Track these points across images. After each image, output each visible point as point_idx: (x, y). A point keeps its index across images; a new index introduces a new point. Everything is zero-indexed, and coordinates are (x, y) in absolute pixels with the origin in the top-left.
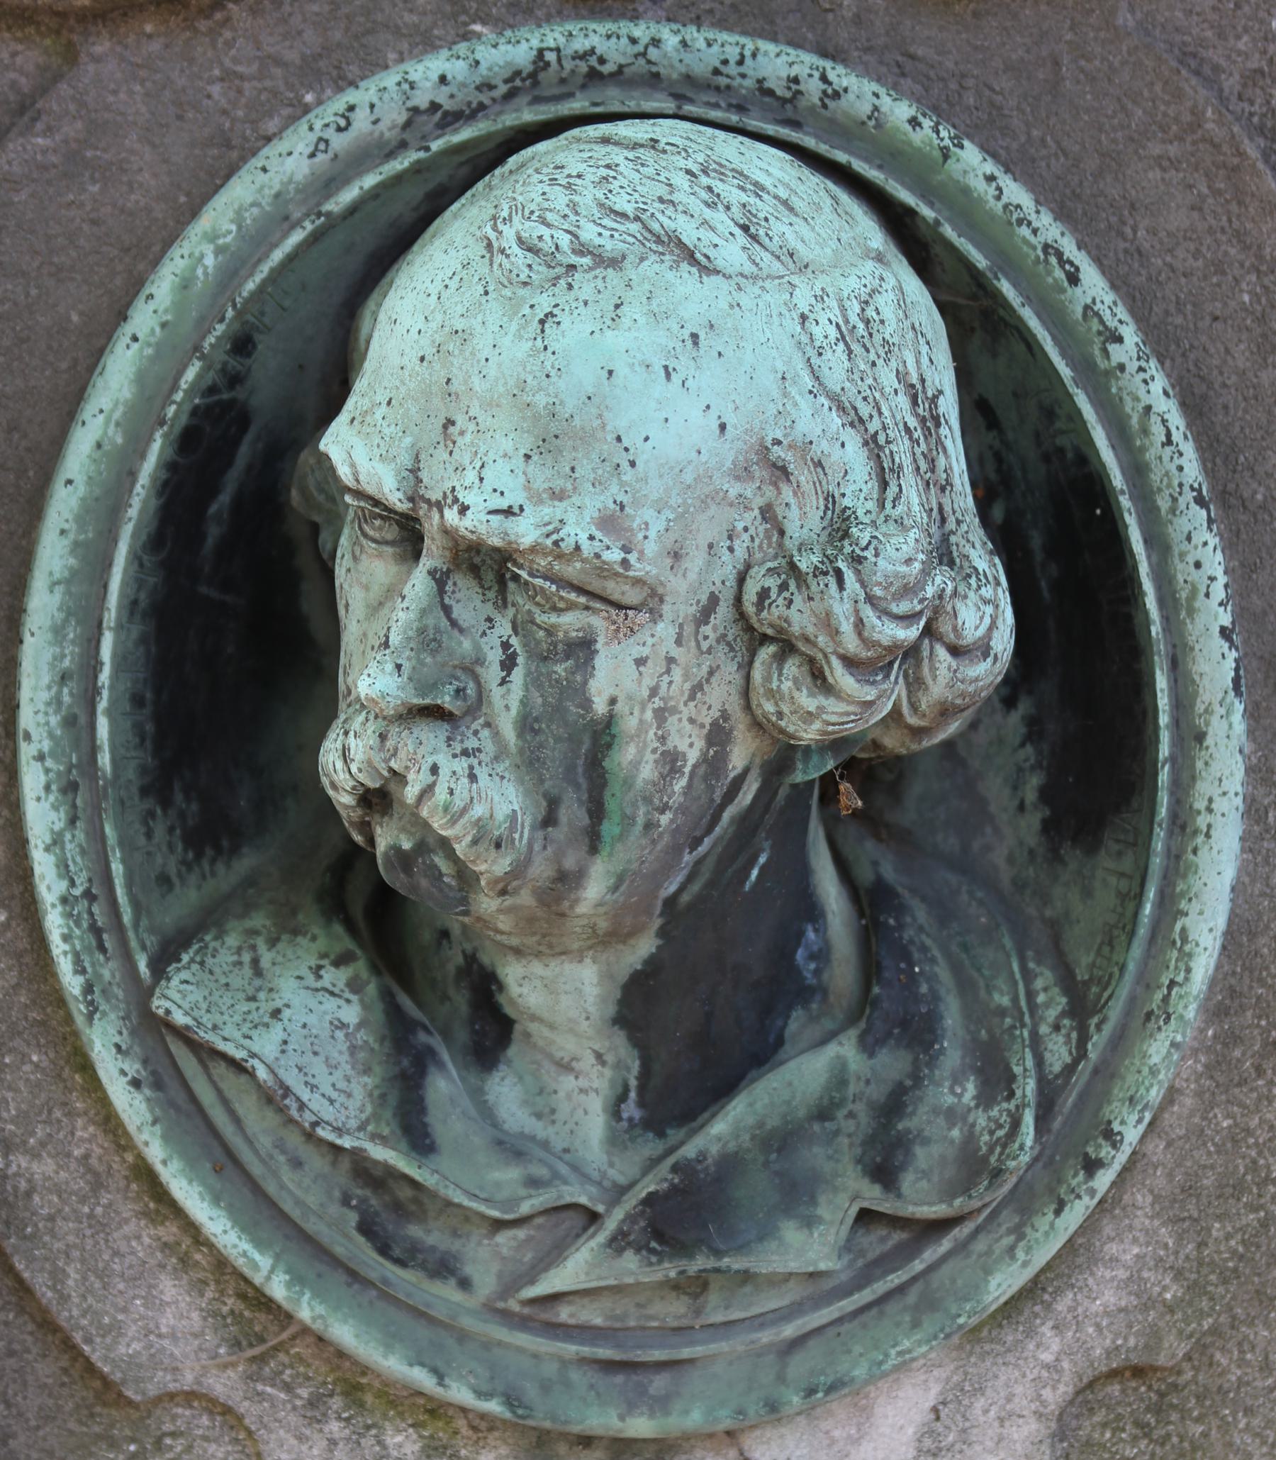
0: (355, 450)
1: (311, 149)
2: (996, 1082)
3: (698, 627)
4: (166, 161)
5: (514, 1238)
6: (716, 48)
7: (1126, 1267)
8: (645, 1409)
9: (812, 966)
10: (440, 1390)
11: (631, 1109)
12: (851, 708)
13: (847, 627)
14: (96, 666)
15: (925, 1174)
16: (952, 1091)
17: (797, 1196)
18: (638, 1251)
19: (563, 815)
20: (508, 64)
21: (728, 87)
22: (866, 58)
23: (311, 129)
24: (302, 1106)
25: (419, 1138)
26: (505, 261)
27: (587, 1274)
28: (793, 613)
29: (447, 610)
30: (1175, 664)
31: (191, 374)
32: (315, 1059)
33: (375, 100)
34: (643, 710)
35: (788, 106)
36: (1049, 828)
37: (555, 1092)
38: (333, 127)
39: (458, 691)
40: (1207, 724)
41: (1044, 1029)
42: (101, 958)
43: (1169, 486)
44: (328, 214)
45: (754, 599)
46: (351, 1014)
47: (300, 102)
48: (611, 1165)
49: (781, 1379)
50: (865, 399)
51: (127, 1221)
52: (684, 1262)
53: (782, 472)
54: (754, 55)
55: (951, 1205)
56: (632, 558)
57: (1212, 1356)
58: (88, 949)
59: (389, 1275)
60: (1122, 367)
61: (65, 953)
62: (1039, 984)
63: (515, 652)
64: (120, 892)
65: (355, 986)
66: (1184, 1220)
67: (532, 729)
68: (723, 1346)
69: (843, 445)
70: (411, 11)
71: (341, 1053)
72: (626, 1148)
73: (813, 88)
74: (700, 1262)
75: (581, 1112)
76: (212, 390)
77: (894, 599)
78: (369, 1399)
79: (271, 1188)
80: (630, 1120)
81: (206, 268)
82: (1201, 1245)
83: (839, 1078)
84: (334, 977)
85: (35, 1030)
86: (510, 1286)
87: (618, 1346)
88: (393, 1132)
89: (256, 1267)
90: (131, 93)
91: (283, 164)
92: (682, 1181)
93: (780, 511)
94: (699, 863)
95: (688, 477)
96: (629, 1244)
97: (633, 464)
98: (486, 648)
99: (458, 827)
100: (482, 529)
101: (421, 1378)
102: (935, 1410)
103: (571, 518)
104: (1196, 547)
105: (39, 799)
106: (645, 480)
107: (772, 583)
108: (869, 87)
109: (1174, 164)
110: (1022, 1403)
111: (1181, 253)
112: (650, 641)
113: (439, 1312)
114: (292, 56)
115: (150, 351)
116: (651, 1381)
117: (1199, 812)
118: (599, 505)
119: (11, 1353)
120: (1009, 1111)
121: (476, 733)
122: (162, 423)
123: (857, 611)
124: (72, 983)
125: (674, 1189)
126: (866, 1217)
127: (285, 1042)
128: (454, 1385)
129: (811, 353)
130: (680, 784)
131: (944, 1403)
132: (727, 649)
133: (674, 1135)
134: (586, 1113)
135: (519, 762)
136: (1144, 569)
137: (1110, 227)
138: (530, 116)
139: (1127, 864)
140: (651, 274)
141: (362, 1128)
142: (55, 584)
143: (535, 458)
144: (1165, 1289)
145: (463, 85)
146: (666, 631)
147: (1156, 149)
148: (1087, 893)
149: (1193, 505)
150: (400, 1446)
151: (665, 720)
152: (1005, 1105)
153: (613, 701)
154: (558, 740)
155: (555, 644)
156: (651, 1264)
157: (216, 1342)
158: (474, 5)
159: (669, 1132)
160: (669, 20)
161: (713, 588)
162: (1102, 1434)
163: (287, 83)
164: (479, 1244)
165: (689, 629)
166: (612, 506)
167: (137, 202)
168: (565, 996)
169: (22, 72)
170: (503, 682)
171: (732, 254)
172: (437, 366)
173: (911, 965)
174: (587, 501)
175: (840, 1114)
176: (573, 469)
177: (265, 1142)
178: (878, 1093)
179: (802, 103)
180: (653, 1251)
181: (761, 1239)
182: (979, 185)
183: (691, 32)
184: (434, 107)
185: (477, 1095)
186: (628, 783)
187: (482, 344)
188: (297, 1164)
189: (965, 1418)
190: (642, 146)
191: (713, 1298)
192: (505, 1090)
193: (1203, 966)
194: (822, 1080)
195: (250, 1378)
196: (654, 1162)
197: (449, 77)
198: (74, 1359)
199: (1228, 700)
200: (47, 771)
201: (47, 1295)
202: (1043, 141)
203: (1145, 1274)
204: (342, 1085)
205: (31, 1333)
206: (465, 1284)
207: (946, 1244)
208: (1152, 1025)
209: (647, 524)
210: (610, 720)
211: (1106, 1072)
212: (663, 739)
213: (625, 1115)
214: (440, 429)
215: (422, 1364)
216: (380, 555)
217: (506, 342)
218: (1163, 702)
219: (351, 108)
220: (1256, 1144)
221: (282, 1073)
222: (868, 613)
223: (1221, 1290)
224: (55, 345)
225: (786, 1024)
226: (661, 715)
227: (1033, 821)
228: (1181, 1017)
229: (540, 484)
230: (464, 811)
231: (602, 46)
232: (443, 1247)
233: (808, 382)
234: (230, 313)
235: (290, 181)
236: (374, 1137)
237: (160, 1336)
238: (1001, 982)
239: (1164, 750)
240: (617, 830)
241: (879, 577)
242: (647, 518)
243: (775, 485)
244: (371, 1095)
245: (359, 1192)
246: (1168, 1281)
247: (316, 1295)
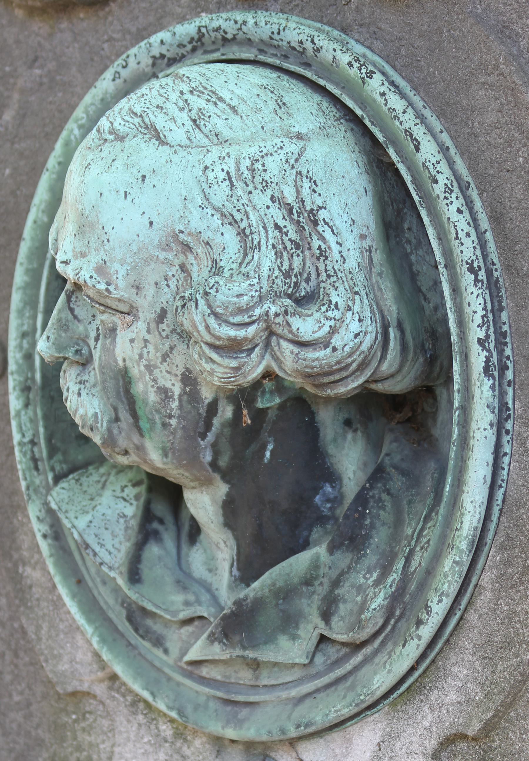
1: (112, 77)
3: (158, 325)
5: (188, 631)
6: (269, 26)
8: (233, 725)
9: (328, 505)
12: (227, 370)
13: (202, 328)
15: (342, 618)
17: (289, 623)
18: (219, 643)
20: (187, 34)
22: (360, 30)
24: (95, 554)
27: (201, 652)
29: (72, 310)
32: (106, 532)
34: (139, 365)
39: (77, 351)
42: (35, 473)
49: (289, 717)
50: (238, 211)
53: (187, 248)
54: (284, 29)
56: (111, 288)
57: (508, 734)
58: (29, 469)
66: (486, 658)
69: (222, 234)
70: (179, 6)
71: (120, 529)
72: (234, 591)
77: (232, 315)
81: (75, 136)
82: (494, 672)
83: (315, 565)
84: (131, 492)
87: (228, 692)
92: (236, 609)
93: (189, 267)
94: (214, 446)
95: (134, 248)
97: (108, 241)
98: (90, 330)
101: (146, 695)
102: (379, 745)
106: (113, 249)
110: (415, 747)
111: (494, 135)
112: (136, 331)
114: (134, 29)
115: (54, 176)
116: (241, 711)
118: (96, 261)
123: (205, 320)
127: (91, 522)
128: (159, 702)
129: (205, 186)
130: (175, 405)
132: (178, 337)
137: (462, 120)
140: (135, 144)
145: (171, 45)
146: (141, 326)
147: (482, 79)
149: (467, 272)
150: (165, 731)
151: (152, 371)
156: (223, 650)
158: (203, 3)
161: (162, 305)
164: (174, 632)
165: (153, 326)
166: (101, 261)
173: (365, 509)
174: (92, 258)
175: (317, 583)
176: (89, 242)
178: (334, 574)
181: (266, 643)
186: (145, 402)
191: (265, 673)
194: (306, 565)
195: (110, 688)
197: (164, 41)
199: (481, 378)
202: (434, 74)
204: (117, 546)
206: (166, 651)
207: (359, 657)
209: (117, 271)
212: (155, 380)
215: (147, 689)
219: (128, 57)
220: (520, 621)
221: (86, 537)
222: (212, 322)
225: (310, 534)
228: (458, 547)
231: (225, 25)
232: (159, 632)
233: (199, 200)
235: (106, 93)
237: (76, 663)
240: (148, 426)
241: (218, 303)
242: (117, 268)
243: (184, 253)
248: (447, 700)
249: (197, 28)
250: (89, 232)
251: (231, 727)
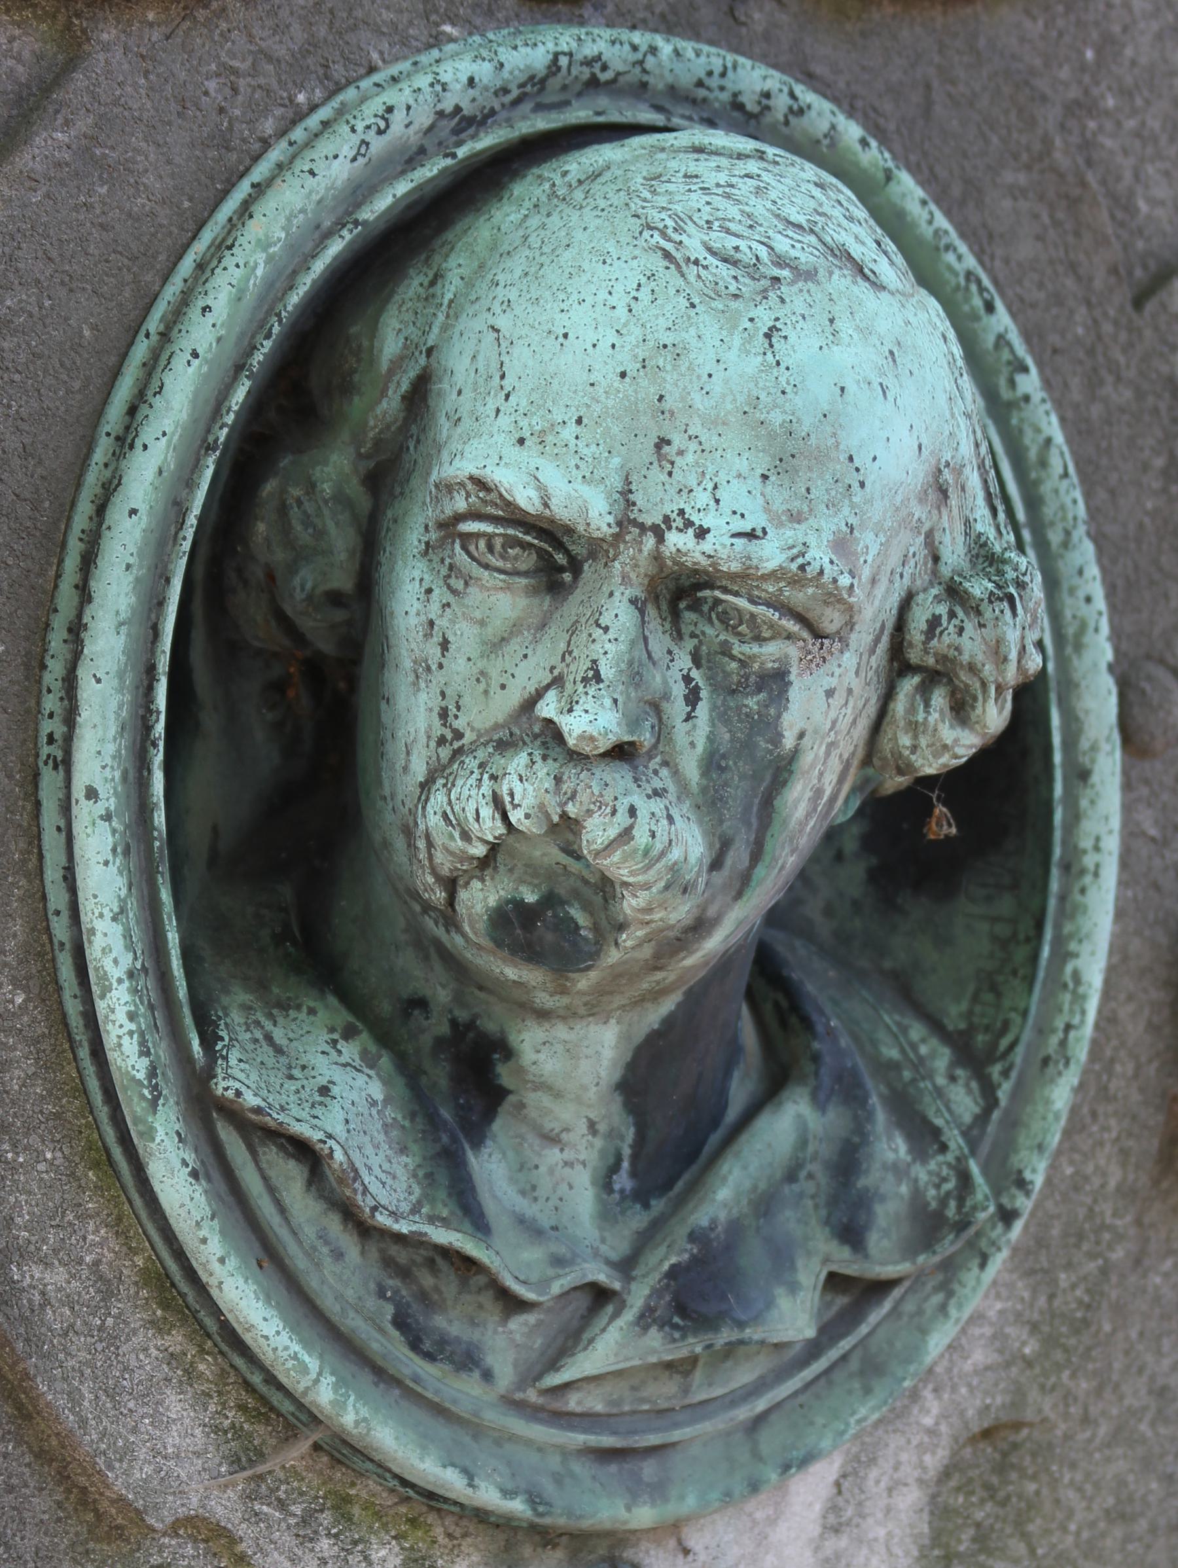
1: (354, 152)
2: (924, 1137)
4: (169, 162)
5: (526, 1324)
6: (703, 59)
7: (991, 1324)
8: (646, 1497)
10: (469, 1491)
11: (623, 1181)
18: (661, 1327)
20: (528, 67)
21: (705, 100)
23: (353, 130)
24: (366, 1190)
26: (703, 272)
28: (965, 641)
33: (411, 102)
35: (753, 122)
36: (874, 877)
37: (537, 1167)
38: (374, 128)
40: (1093, 761)
43: (1064, 519)
44: (365, 223)
45: (924, 626)
46: (377, 1091)
47: (291, 101)
48: (603, 1241)
49: (757, 1456)
51: (135, 1332)
52: (710, 1336)
54: (735, 67)
55: (914, 1263)
59: (419, 1370)
60: (1027, 398)
61: (131, 1033)
63: (697, 686)
65: (369, 1061)
67: (720, 767)
68: (706, 1427)
73: (781, 103)
74: (726, 1335)
75: (565, 1187)
78: (356, 1511)
79: (312, 1283)
80: (622, 1191)
82: (1051, 1297)
85: (51, 1123)
86: (530, 1376)
88: (452, 1213)
89: (305, 1370)
90: (135, 85)
91: (329, 168)
92: (700, 1251)
96: (654, 1321)
97: (862, 485)
98: (671, 682)
99: (652, 872)
100: (723, 553)
104: (1087, 582)
105: (106, 863)
106: (869, 501)
107: (942, 610)
110: (909, 1472)
113: (463, 1409)
114: (281, 52)
117: (1085, 852)
118: (834, 528)
119: (10, 1489)
120: (949, 1165)
121: (656, 772)
122: (210, 448)
125: (694, 1260)
126: (835, 1282)
128: (483, 1485)
131: (844, 1476)
134: (571, 1187)
135: (700, 801)
138: (542, 123)
139: (1006, 905)
141: (415, 1210)
142: (121, 624)
143: (773, 478)
144: (1024, 1344)
145: (486, 89)
152: (940, 1158)
153: (801, 735)
154: (742, 777)
155: (747, 677)
156: (674, 1340)
157: (217, 1460)
159: (653, 1202)
160: (608, 26)
162: (956, 1499)
163: (280, 81)
164: (495, 1332)
166: (844, 528)
167: (144, 206)
168: (573, 1060)
169: (19, 59)
170: (689, 718)
172: (644, 383)
174: (823, 523)
176: (808, 490)
177: (309, 1232)
179: (768, 119)
180: (675, 1327)
183: (681, 44)
187: (703, 358)
188: (338, 1255)
189: (863, 1492)
190: (748, 156)
191: (698, 1375)
192: (494, 1166)
195: (250, 1497)
197: (477, 80)
198: (68, 1491)
200: (114, 831)
203: (1008, 1330)
204: (386, 1166)
205: (28, 1465)
208: (1051, 1069)
211: (1012, 1123)
213: (617, 1187)
214: (652, 449)
215: (453, 1465)
216: (508, 588)
217: (732, 356)
219: (390, 110)
223: (1072, 1341)
224: (68, 363)
229: (778, 506)
230: (663, 854)
234: (276, 329)
236: (432, 1219)
239: (1058, 789)
242: (868, 541)
244: (415, 1176)
245: (391, 1282)
246: (1024, 1337)
247: (359, 1397)
248: (968, 1366)
249: (551, 57)
250: (810, 469)
251: (645, 1503)
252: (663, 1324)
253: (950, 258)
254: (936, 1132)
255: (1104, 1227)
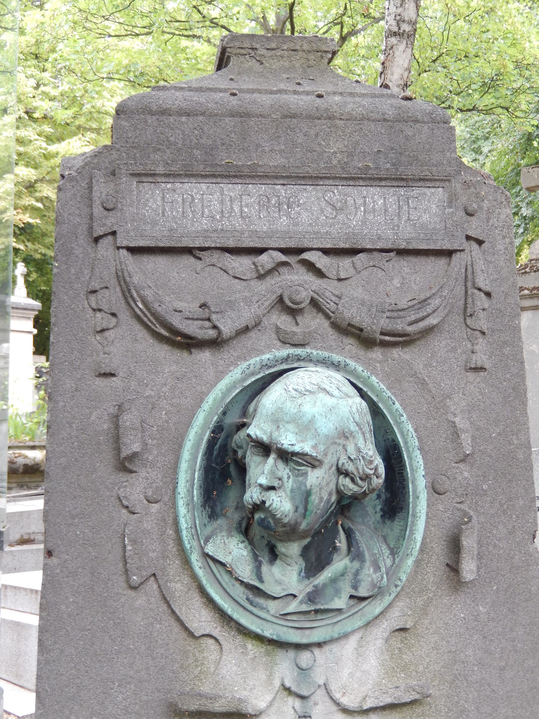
0: (257, 430)
2: (377, 568)
11: (303, 574)
14: (194, 479)
15: (364, 588)
16: (368, 571)
17: (338, 592)
19: (299, 510)
25: (261, 580)
29: (276, 466)
30: (413, 482)
31: (215, 418)
41: (385, 558)
62: (383, 548)
64: (198, 527)
65: (246, 547)
73: (343, 363)
76: (218, 422)
84: (241, 545)
103: (306, 446)
108: (354, 364)
109: (411, 382)
124: (188, 546)
125: (313, 591)
126: (352, 597)
130: (322, 504)
133: (311, 579)
136: (407, 463)
139: (402, 523)
147: (407, 379)
148: (392, 530)
171: (336, 393)
178: (353, 571)
179: (340, 366)
182: (375, 384)
184: (267, 365)
185: (270, 570)
186: (313, 503)
193: (418, 545)
196: (307, 585)
201: (179, 614)
210: (310, 490)
211: (399, 567)
218: (411, 490)
226: (321, 489)
227: (379, 515)
229: (299, 439)
238: (375, 548)
239: (411, 500)
252: (306, 603)
253: (384, 394)
254: (380, 568)
255: (429, 589)
